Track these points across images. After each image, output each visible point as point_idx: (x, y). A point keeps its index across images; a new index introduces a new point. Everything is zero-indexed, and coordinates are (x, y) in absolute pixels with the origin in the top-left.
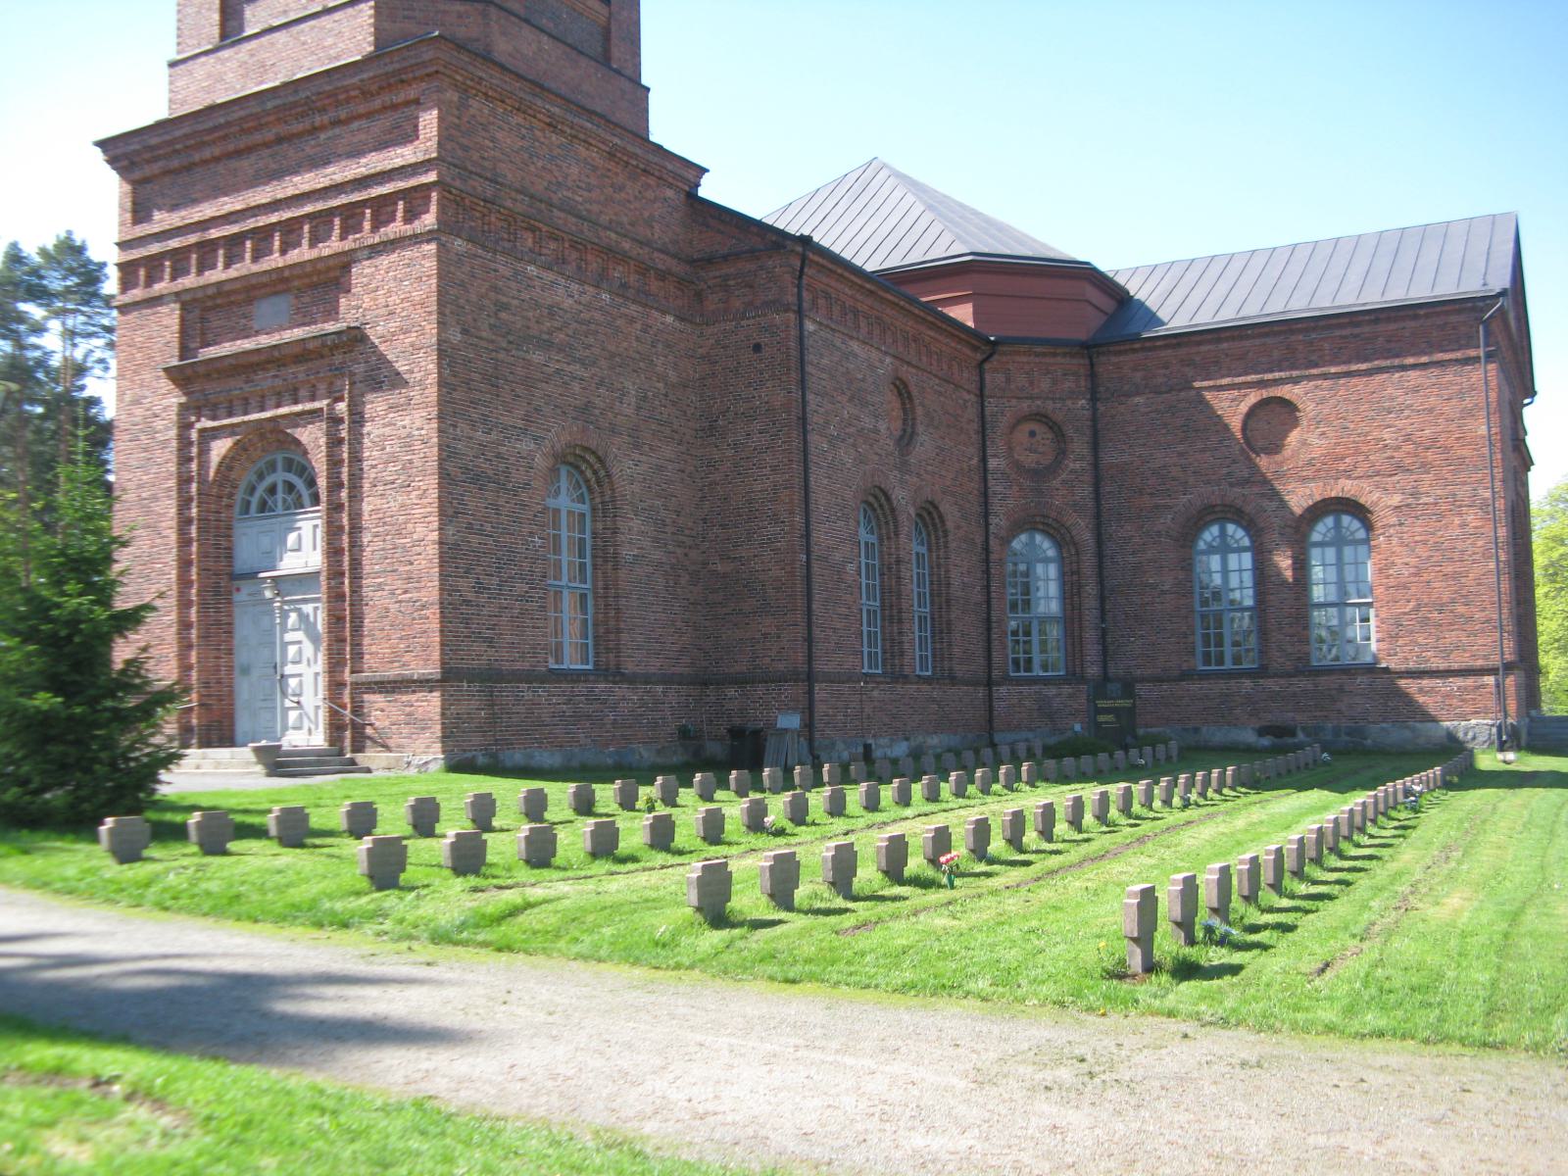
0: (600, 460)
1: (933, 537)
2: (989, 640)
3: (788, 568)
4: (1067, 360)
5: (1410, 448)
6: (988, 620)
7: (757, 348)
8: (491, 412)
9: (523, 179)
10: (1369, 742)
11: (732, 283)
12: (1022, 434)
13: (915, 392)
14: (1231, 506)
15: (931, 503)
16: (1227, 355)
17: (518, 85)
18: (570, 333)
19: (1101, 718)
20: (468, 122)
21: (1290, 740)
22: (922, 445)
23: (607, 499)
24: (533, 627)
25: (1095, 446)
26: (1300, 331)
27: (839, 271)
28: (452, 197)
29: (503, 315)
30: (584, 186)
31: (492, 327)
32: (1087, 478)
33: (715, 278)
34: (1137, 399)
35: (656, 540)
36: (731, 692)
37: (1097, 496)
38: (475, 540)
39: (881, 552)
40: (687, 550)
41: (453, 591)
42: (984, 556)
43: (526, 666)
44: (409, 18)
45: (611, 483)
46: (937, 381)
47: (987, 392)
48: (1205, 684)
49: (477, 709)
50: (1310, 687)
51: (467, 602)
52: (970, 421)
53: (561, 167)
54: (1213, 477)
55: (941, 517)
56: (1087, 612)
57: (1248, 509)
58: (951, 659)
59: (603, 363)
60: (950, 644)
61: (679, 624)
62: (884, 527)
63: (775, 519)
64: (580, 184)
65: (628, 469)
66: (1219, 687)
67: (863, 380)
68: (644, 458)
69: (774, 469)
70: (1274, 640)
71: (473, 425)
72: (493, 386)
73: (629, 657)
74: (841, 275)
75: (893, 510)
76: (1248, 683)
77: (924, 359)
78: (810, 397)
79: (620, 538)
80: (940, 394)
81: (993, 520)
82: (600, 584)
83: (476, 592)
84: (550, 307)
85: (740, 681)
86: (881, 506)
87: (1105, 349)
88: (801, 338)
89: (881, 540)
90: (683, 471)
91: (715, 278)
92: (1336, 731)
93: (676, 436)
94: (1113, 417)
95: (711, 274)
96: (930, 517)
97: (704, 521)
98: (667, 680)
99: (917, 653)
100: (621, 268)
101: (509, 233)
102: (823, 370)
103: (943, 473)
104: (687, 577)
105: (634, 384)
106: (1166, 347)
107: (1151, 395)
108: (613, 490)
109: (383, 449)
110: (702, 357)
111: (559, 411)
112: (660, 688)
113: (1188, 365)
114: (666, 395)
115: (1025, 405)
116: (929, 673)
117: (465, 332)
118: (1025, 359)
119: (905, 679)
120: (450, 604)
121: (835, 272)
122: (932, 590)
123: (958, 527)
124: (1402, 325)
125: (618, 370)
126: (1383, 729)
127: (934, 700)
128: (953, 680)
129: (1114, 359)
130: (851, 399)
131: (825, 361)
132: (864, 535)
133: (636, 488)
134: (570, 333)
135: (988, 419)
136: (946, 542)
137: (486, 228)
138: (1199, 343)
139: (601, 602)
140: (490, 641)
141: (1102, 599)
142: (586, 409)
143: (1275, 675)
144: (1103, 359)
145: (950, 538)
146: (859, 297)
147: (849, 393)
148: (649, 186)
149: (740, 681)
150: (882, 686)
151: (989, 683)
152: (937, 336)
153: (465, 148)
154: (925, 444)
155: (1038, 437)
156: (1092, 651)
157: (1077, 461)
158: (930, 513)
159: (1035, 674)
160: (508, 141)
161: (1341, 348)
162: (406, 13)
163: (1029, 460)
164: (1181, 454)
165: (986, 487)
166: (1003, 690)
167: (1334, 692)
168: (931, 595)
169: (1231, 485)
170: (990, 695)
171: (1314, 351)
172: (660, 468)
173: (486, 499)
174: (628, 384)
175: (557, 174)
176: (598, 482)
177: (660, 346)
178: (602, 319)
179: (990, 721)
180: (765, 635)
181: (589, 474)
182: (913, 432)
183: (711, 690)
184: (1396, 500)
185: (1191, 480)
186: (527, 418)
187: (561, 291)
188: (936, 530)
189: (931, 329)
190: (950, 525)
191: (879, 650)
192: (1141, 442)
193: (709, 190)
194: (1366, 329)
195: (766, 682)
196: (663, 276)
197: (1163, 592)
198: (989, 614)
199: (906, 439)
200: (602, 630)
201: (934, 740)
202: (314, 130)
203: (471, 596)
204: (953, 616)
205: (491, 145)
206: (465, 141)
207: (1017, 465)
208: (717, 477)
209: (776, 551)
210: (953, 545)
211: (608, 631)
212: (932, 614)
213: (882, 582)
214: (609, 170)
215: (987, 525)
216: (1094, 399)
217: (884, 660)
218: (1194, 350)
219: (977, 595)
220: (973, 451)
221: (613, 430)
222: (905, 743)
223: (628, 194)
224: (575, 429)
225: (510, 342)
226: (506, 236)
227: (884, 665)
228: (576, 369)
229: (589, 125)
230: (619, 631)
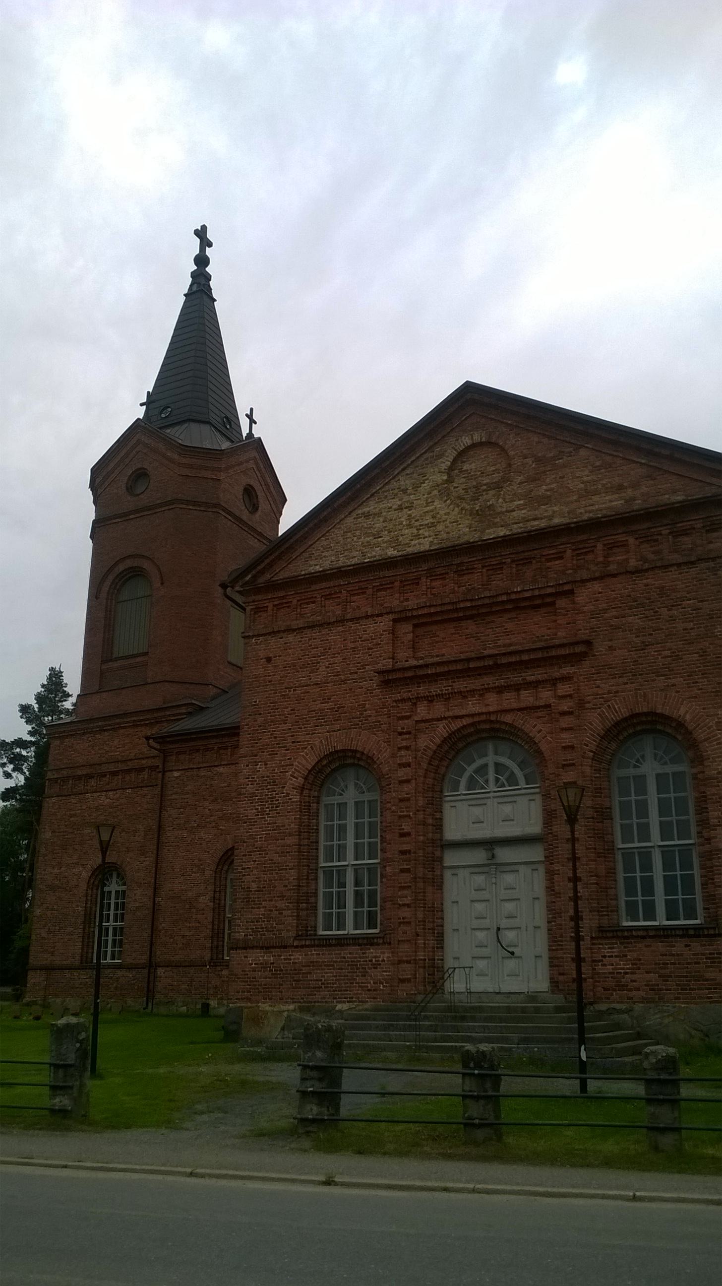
38: (49, 913)
43: (68, 962)
51: (43, 938)
117: (53, 832)
140: (52, 953)
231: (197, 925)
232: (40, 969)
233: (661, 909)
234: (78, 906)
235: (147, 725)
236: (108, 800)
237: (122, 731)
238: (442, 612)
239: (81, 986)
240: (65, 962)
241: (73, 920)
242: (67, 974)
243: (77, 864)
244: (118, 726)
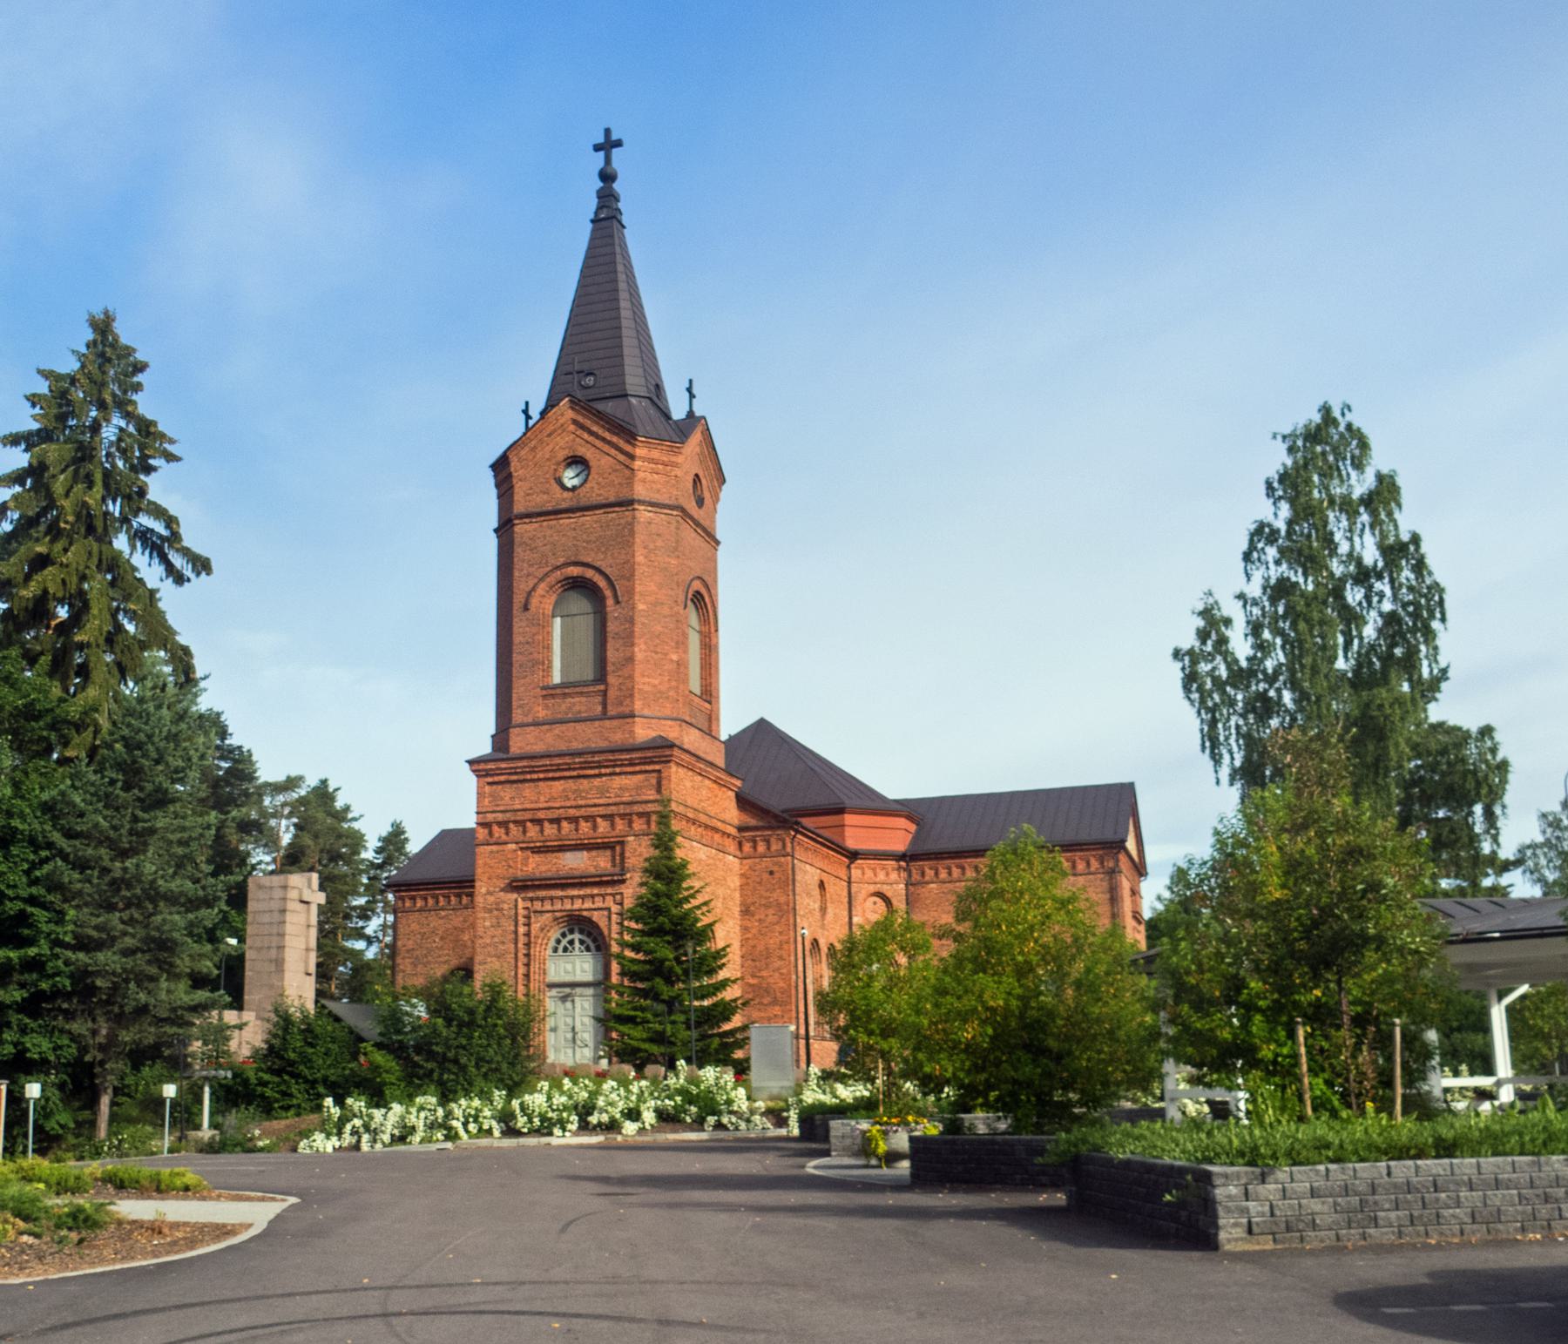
34: (932, 886)
69: (780, 933)
202: (600, 775)
208: (749, 935)
220: (846, 913)
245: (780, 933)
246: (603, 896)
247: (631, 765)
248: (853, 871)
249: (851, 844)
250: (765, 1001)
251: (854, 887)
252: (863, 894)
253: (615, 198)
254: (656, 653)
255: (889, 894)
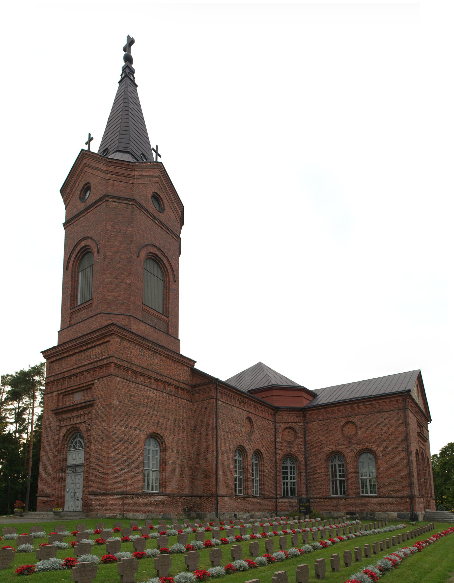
0: (161, 436)
1: (260, 459)
2: (276, 487)
3: (212, 466)
4: (298, 413)
5: (385, 435)
6: (276, 482)
7: (206, 408)
8: (127, 423)
9: (140, 362)
10: (376, 517)
11: (201, 391)
12: (286, 432)
13: (253, 421)
14: (338, 451)
15: (258, 450)
16: (337, 410)
17: (138, 338)
18: (153, 403)
19: (301, 508)
20: (123, 347)
21: (355, 516)
22: (256, 434)
23: (164, 447)
24: (138, 480)
25: (305, 435)
26: (356, 403)
27: (229, 388)
28: (117, 366)
29: (132, 398)
30: (159, 365)
31: (129, 401)
32: (303, 444)
33: (197, 390)
34: (315, 423)
35: (178, 458)
36: (198, 499)
37: (305, 449)
38: (120, 456)
39: (243, 462)
40: (187, 461)
41: (113, 470)
42: (275, 464)
43: (135, 490)
44: (109, 319)
45: (165, 443)
46: (261, 418)
47: (276, 421)
48: (332, 500)
49: (119, 502)
50: (360, 501)
51: (117, 473)
52: (271, 429)
53: (152, 360)
54: (334, 443)
55: (262, 454)
56: (302, 480)
57: (343, 452)
58: (264, 491)
59: (164, 412)
60: (264, 487)
61: (185, 480)
62: (244, 456)
63: (209, 453)
64: (158, 364)
65: (170, 440)
66: (335, 501)
67: (237, 417)
68: (175, 437)
69: (209, 440)
70: (350, 488)
71: (121, 426)
72: (128, 416)
73: (168, 489)
74: (230, 389)
75: (246, 452)
76: (343, 500)
77: (257, 412)
78: (219, 421)
79: (167, 457)
80: (262, 421)
81: (278, 455)
82: (161, 469)
83: (120, 471)
84: (147, 396)
85: (200, 496)
86: (243, 450)
87: (307, 409)
88: (217, 405)
89: (243, 459)
90: (187, 440)
91: (197, 390)
92: (367, 514)
93: (186, 431)
94: (309, 427)
95: (197, 389)
96: (258, 453)
97: (193, 453)
98: (180, 496)
99: (254, 491)
100: (170, 387)
101: (135, 376)
102: (224, 414)
103: (263, 442)
104: (188, 468)
105: (173, 417)
106: (322, 408)
107: (318, 422)
108: (165, 445)
109: (98, 432)
110: (194, 411)
111: (149, 423)
112: (178, 498)
113: (328, 413)
114: (183, 420)
115: (286, 424)
116: (258, 495)
117: (119, 402)
118: (286, 412)
119: (248, 497)
120: (111, 474)
121: (228, 389)
122: (259, 473)
123: (267, 456)
124: (383, 401)
125: (168, 413)
126: (379, 514)
127: (258, 502)
128: (264, 497)
129: (310, 412)
130: (233, 422)
131: (224, 412)
132: (237, 458)
133: (173, 444)
134: (153, 403)
135: (277, 428)
136: (263, 460)
137: (128, 375)
138: (330, 407)
139: (161, 474)
140: (124, 484)
141: (306, 476)
142: (157, 423)
143: (350, 498)
144: (307, 412)
145: (264, 459)
146: (236, 395)
147: (232, 420)
148: (179, 366)
149: (200, 496)
150: (241, 498)
151: (276, 499)
152: (261, 406)
153: (122, 354)
154: (257, 434)
155: (290, 433)
156: (304, 490)
157: (300, 440)
158: (258, 453)
159: (289, 496)
160: (136, 352)
161: (367, 408)
162: (109, 318)
163: (288, 439)
164: (326, 437)
165: (276, 446)
166: (280, 500)
167: (366, 503)
168: (259, 474)
169: (339, 445)
170: (276, 502)
171: (360, 408)
172: (180, 439)
173: (125, 446)
174: (171, 417)
175: (150, 361)
176: (161, 442)
177: (181, 408)
178: (163, 400)
179: (276, 508)
180: (206, 484)
181: (159, 440)
182: (253, 431)
183: (193, 499)
184: (381, 449)
185: (328, 444)
186: (139, 425)
187: (151, 392)
188: (261, 457)
189: (259, 404)
190: (264, 456)
191: (242, 489)
192: (316, 434)
193: (196, 366)
194: (374, 402)
195: (206, 496)
196: (183, 389)
197: (322, 474)
198: (276, 479)
199: (252, 432)
200: (161, 482)
201: (258, 513)
202: (88, 349)
203: (118, 471)
204: (265, 480)
205: (130, 353)
206: (122, 352)
207: (285, 441)
208: (196, 442)
209: (209, 461)
210: (265, 461)
211: (163, 482)
212: (259, 479)
213: (243, 470)
214: (167, 361)
215: (276, 456)
216: (304, 423)
217: (243, 491)
218: (329, 409)
219: (273, 474)
220: (272, 436)
221: (166, 429)
222: (249, 514)
223: (173, 367)
224: (154, 428)
225: (134, 405)
226: (134, 377)
227: (243, 493)
228: (155, 413)
229: (160, 349)
230: (165, 482)
231: (230, 478)
232: (116, 494)
233: (369, 492)
234: (139, 455)
235: (172, 360)
236: (154, 395)
237: (159, 356)
238: (94, 338)
239: (144, 505)
240: (133, 490)
241: (137, 464)
242: (135, 498)
243: (138, 428)
244: (158, 352)
245: (209, 440)
246: (80, 416)
247: (98, 340)
248: (277, 417)
249: (276, 404)
250: (202, 477)
251: (277, 425)
252: (281, 429)
253: (132, 72)
254: (117, 279)
255: (295, 427)
